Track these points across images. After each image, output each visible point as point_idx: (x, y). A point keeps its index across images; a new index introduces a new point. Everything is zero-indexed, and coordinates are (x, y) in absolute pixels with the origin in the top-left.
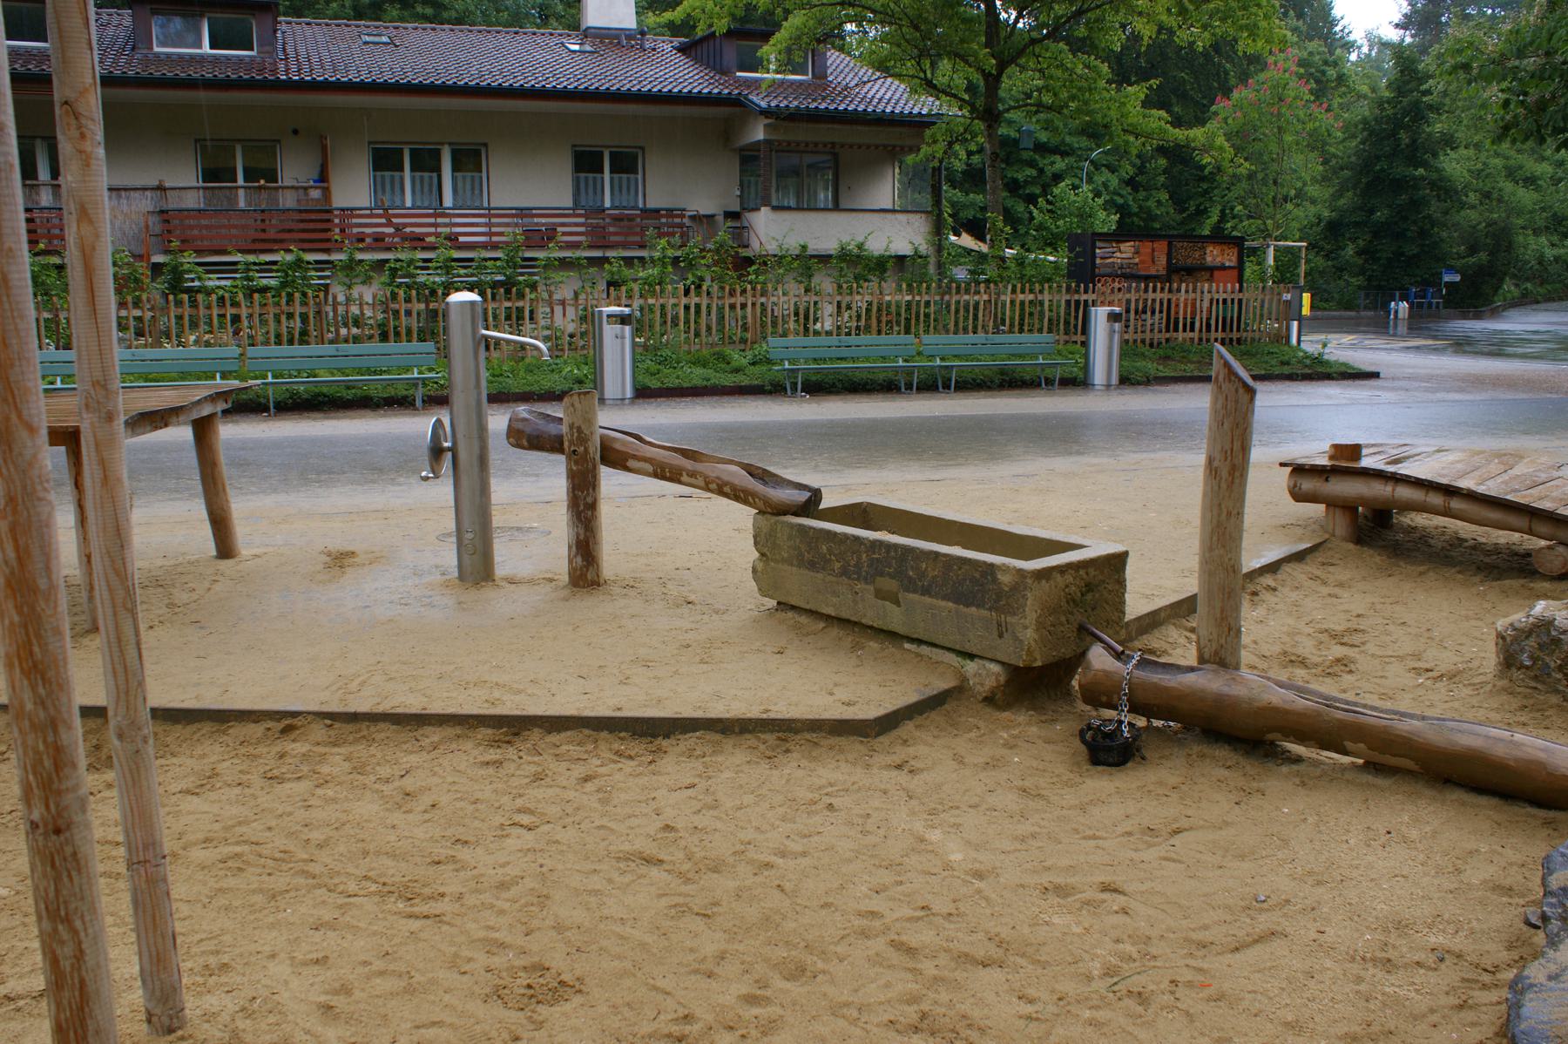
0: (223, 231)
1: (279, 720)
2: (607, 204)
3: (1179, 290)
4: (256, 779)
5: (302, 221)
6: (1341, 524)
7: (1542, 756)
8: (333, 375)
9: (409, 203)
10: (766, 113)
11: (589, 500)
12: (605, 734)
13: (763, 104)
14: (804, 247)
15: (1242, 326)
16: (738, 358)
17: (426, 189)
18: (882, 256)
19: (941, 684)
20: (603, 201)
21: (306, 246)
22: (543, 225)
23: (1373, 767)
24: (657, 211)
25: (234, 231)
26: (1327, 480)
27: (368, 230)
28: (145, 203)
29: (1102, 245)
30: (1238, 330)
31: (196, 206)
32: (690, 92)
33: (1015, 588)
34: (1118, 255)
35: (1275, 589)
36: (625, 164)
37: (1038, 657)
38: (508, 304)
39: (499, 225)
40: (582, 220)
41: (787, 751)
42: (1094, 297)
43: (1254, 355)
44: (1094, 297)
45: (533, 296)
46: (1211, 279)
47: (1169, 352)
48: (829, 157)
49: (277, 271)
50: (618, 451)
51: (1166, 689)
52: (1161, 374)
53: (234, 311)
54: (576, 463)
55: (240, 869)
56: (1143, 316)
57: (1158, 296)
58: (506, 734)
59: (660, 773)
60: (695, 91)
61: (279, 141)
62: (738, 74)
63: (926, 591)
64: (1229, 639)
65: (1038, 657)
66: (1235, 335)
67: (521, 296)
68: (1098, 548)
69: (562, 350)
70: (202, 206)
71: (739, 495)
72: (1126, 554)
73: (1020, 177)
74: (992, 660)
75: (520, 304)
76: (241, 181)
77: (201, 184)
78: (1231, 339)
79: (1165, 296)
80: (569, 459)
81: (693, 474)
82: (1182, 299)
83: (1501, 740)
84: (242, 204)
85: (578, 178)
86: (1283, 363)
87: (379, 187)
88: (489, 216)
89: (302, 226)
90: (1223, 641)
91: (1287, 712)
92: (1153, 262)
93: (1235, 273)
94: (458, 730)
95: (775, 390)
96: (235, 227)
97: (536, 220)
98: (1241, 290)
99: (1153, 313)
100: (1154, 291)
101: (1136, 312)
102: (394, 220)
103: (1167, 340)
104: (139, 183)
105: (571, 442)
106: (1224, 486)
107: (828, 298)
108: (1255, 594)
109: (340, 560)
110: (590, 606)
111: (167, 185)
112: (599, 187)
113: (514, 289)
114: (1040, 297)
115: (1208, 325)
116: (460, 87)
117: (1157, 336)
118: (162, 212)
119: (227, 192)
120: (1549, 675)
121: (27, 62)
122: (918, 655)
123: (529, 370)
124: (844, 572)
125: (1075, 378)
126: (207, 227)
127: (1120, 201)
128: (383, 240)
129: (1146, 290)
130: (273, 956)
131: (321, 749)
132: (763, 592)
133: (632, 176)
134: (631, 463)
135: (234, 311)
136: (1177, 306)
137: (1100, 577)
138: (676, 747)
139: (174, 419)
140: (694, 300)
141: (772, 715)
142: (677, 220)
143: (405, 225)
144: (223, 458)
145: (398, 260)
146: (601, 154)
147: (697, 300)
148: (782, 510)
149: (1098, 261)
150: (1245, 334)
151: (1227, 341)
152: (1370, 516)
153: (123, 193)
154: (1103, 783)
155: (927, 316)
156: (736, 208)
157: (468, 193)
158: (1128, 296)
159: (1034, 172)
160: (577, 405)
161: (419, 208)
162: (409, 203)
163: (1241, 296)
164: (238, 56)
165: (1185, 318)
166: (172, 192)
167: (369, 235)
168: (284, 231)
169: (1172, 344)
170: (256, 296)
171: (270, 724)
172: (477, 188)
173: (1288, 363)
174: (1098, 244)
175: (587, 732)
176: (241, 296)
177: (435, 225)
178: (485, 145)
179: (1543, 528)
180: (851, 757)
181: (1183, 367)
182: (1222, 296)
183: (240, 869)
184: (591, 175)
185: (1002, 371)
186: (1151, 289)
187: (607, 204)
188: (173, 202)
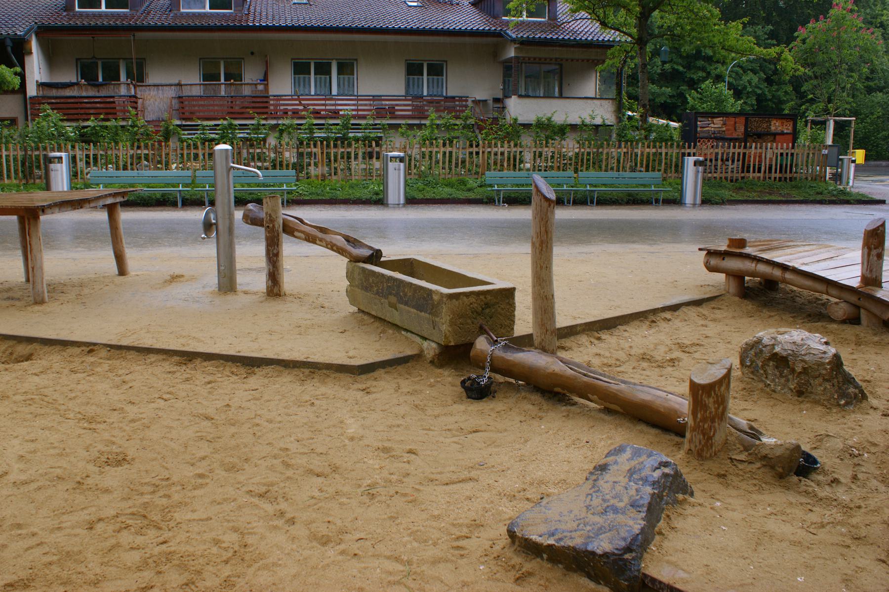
0: (211, 108)
1: (88, 347)
2: (425, 93)
3: (751, 147)
4: (66, 371)
5: (253, 102)
6: (733, 287)
7: (677, 406)
8: (243, 187)
9: (313, 93)
10: (514, 41)
11: (275, 252)
12: (230, 363)
13: (514, 36)
14: (516, 120)
15: (794, 169)
16: (472, 183)
17: (323, 84)
18: (562, 125)
19: (409, 352)
20: (423, 92)
21: (234, 116)
22: (386, 105)
23: (608, 411)
24: (453, 98)
25: (216, 108)
26: (723, 259)
27: (290, 108)
28: (171, 93)
29: (701, 119)
30: (791, 172)
31: (198, 94)
32: (472, 29)
33: (440, 302)
34: (712, 125)
35: (669, 320)
36: (436, 70)
37: (452, 340)
38: (343, 150)
39: (361, 105)
40: (410, 103)
41: (313, 378)
42: (694, 151)
43: (800, 188)
44: (694, 151)
45: (356, 146)
46: (774, 140)
47: (743, 185)
48: (557, 67)
49: (219, 130)
50: (290, 227)
51: (508, 361)
52: (732, 198)
53: (195, 151)
54: (269, 232)
55: (30, 405)
56: (726, 163)
57: (737, 151)
58: (185, 360)
59: (247, 383)
60: (481, 28)
61: (243, 59)
62: (503, 18)
63: (406, 304)
64: (547, 336)
65: (452, 340)
66: (788, 175)
67: (350, 145)
68: (499, 284)
69: (372, 176)
70: (202, 94)
71: (341, 251)
72: (514, 289)
73: (695, 77)
74: (433, 341)
75: (349, 150)
76: (222, 81)
77: (202, 82)
78: (786, 178)
79: (742, 151)
80: (266, 230)
81: (321, 240)
82: (753, 153)
83: (661, 397)
84: (223, 93)
85: (409, 79)
86: (818, 193)
87: (297, 84)
88: (358, 100)
89: (254, 105)
90: (543, 337)
91: (562, 376)
92: (735, 130)
93: (790, 137)
94: (164, 357)
95: (489, 201)
96: (217, 105)
97: (383, 102)
98: (793, 147)
99: (733, 161)
100: (734, 147)
101: (722, 160)
102: (303, 102)
103: (743, 178)
104: (168, 82)
105: (267, 222)
106: (538, 252)
107: (528, 149)
108: (653, 322)
109: (175, 278)
110: (275, 305)
111: (183, 83)
112: (421, 83)
113: (346, 142)
114: (659, 151)
115: (770, 168)
116: (341, 28)
117: (735, 175)
118: (180, 97)
119: (213, 87)
120: (757, 371)
121: (117, 20)
122: (406, 338)
123: (352, 187)
124: (377, 293)
125: (676, 199)
126: (202, 105)
127: (759, 92)
128: (298, 113)
129: (729, 147)
130: (17, 437)
131: (101, 361)
132: (353, 301)
133: (440, 77)
134: (296, 234)
135: (195, 151)
136: (750, 157)
137: (495, 300)
138: (260, 372)
139: (87, 205)
140: (475, 150)
141: (309, 360)
142: (464, 103)
143: (309, 105)
144: (121, 227)
145: (284, 125)
146: (422, 65)
147: (450, 149)
148: (355, 260)
149: (699, 129)
150: (795, 175)
151: (783, 179)
152: (763, 283)
153: (160, 87)
154: (475, 407)
155: (588, 160)
156: (500, 96)
157: (346, 86)
158: (716, 150)
159: (704, 75)
160: (269, 203)
161: (318, 95)
162: (313, 93)
163: (793, 151)
164: (223, 13)
165: (776, 165)
166: (186, 87)
167: (290, 110)
168: (243, 108)
169: (745, 180)
170: (207, 143)
171: (84, 348)
172: (351, 85)
173: (821, 193)
174: (699, 119)
175: (222, 361)
176: (199, 143)
177: (325, 105)
178: (356, 60)
179: (834, 292)
180: (342, 384)
181: (748, 194)
182: (779, 151)
183: (30, 405)
184: (435, 77)
185: (630, 195)
186: (731, 147)
187: (425, 93)
188: (186, 92)
